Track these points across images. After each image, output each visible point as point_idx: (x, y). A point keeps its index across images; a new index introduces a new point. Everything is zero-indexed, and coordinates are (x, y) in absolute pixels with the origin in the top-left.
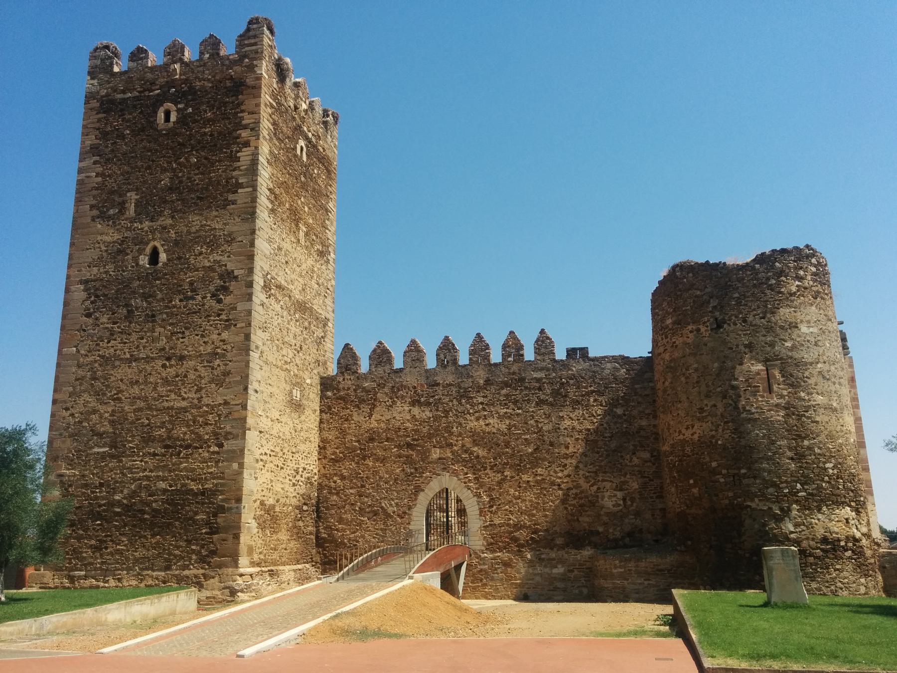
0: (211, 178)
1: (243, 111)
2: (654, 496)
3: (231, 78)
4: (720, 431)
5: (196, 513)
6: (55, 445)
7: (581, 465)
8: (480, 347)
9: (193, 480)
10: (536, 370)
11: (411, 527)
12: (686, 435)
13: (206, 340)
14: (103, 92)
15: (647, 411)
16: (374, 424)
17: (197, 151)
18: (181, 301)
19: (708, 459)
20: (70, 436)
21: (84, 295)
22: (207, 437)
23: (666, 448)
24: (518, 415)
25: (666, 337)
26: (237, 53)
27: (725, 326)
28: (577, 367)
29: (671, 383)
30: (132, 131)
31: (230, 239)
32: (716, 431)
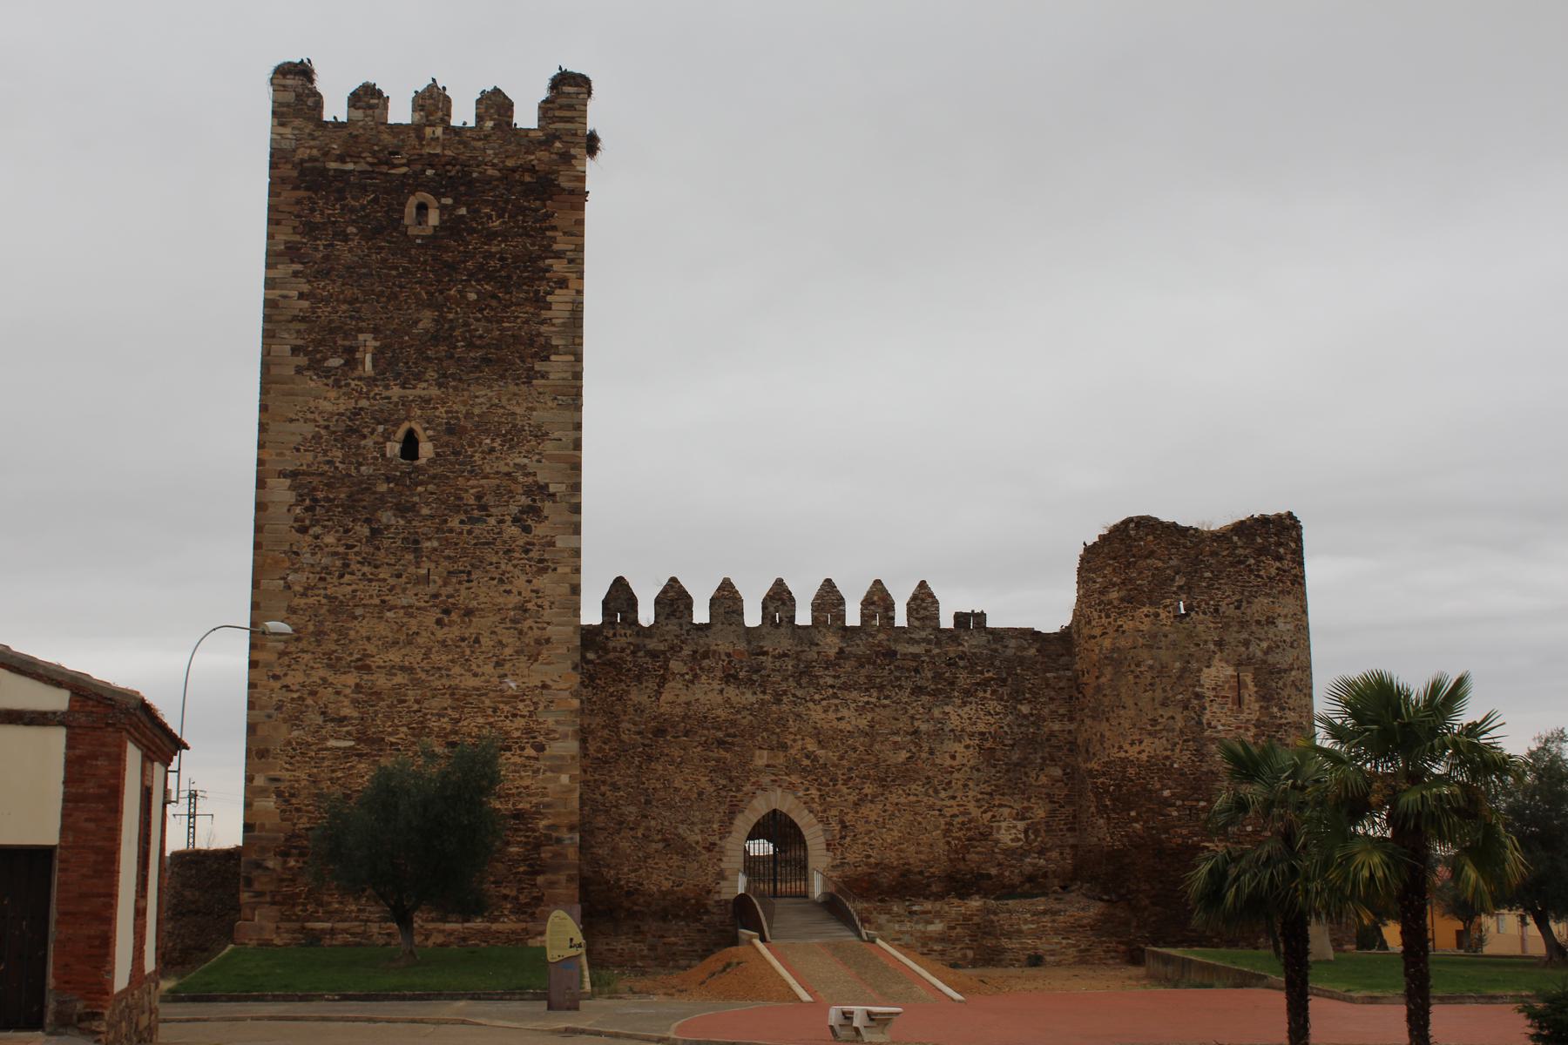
0: (504, 330)
1: (554, 228)
3: (532, 170)
5: (508, 843)
6: (262, 731)
7: (971, 784)
8: (829, 599)
11: (723, 865)
13: (508, 587)
14: (303, 153)
15: (1061, 711)
16: (665, 709)
17: (478, 281)
18: (462, 522)
19: (1158, 786)
20: (285, 721)
21: (290, 497)
23: (1093, 765)
24: (884, 706)
28: (970, 643)
30: (361, 230)
31: (541, 435)
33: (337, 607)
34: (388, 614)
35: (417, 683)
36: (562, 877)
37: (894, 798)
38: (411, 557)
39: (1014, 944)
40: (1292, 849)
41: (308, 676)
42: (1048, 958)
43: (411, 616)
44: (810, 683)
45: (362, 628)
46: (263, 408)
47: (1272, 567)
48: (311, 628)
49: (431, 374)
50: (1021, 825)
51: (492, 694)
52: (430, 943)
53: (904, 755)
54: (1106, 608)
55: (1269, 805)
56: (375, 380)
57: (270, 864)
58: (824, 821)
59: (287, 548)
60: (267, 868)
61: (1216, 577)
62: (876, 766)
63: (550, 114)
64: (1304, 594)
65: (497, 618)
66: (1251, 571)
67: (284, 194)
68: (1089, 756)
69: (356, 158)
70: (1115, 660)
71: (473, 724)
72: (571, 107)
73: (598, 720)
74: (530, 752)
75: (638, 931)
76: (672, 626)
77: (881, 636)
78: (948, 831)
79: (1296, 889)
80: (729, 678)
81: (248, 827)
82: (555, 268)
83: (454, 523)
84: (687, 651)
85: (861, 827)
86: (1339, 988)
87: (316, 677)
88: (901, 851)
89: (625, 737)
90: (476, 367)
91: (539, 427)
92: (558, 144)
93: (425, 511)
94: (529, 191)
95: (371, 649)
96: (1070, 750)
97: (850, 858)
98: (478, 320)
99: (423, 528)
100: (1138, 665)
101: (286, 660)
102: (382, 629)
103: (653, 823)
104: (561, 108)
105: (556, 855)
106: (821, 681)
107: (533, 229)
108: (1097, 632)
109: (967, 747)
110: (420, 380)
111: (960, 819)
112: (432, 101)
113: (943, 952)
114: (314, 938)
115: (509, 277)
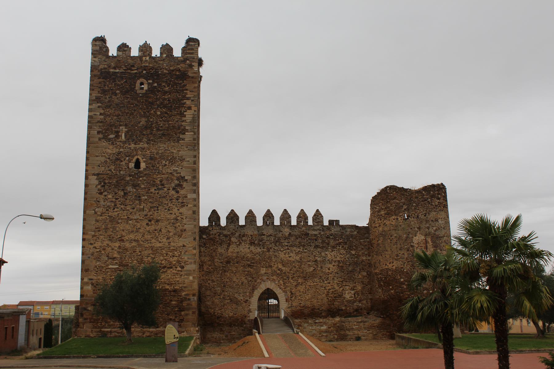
1: (187, 90)
3: (179, 70)
5: (171, 301)
6: (86, 263)
7: (335, 278)
8: (286, 216)
9: (168, 284)
10: (314, 230)
11: (250, 307)
13: (171, 212)
14: (102, 67)
15: (366, 253)
16: (230, 254)
17: (161, 108)
18: (155, 190)
20: (95, 259)
21: (97, 182)
22: (174, 263)
23: (377, 271)
26: (182, 56)
28: (334, 230)
30: (121, 92)
33: (112, 220)
34: (130, 222)
35: (140, 245)
36: (191, 312)
37: (309, 284)
38: (138, 202)
39: (350, 333)
40: (445, 295)
41: (103, 243)
42: (363, 338)
43: (138, 222)
44: (280, 245)
45: (121, 227)
46: (88, 152)
47: (436, 202)
48: (103, 227)
49: (145, 140)
50: (353, 292)
51: (166, 249)
52: (145, 335)
53: (312, 269)
54: (380, 217)
55: (435, 278)
56: (126, 142)
57: (89, 309)
58: (285, 292)
59: (95, 199)
60: (88, 310)
61: (417, 205)
62: (303, 272)
63: (185, 52)
64: (448, 211)
65: (167, 223)
66: (429, 203)
67: (95, 80)
68: (376, 268)
69: (120, 67)
70: (383, 235)
71: (159, 259)
72: (192, 49)
73: (207, 258)
74: (179, 269)
75: (222, 330)
76: (232, 226)
77: (304, 228)
78: (328, 294)
79: (447, 313)
80: (252, 243)
81: (82, 296)
82: (187, 103)
83: (152, 190)
84: (237, 234)
85: (298, 294)
86: (464, 348)
87: (105, 244)
88: (312, 301)
89: (216, 264)
90: (160, 137)
91: (182, 157)
92: (188, 62)
93: (143, 186)
94: (178, 77)
95: (124, 234)
96: (369, 266)
97: (294, 304)
98: (161, 121)
99: (142, 192)
100: (391, 236)
101: (95, 238)
102: (128, 227)
103: (226, 293)
104: (189, 49)
105: (188, 305)
106: (283, 244)
107: (179, 90)
108: (377, 225)
109: (334, 266)
110: (141, 142)
111: (332, 290)
112: (145, 48)
113: (326, 336)
114: (104, 335)
115: (171, 106)
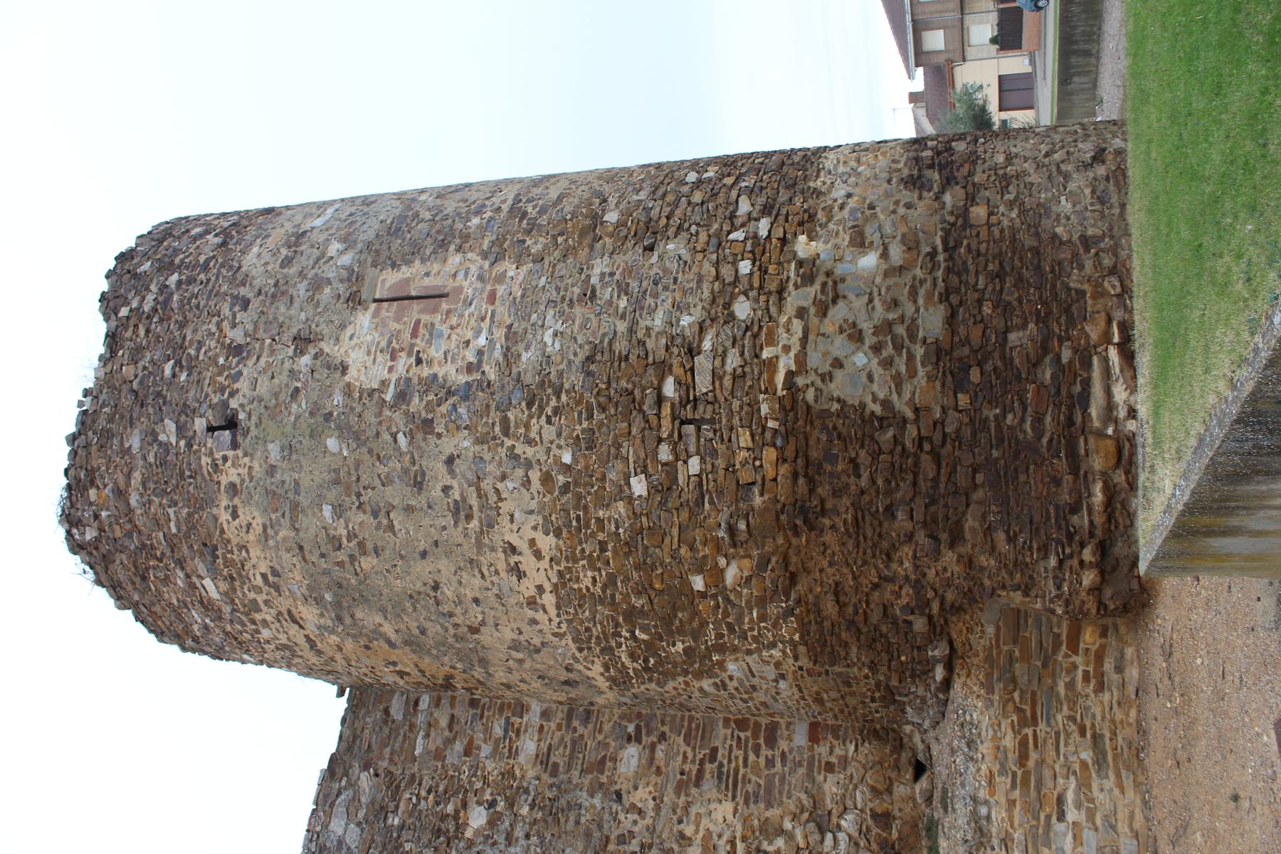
2: (765, 752)
4: (530, 451)
12: (541, 579)
15: (498, 731)
25: (255, 606)
27: (234, 404)
29: (383, 611)
32: (529, 465)
